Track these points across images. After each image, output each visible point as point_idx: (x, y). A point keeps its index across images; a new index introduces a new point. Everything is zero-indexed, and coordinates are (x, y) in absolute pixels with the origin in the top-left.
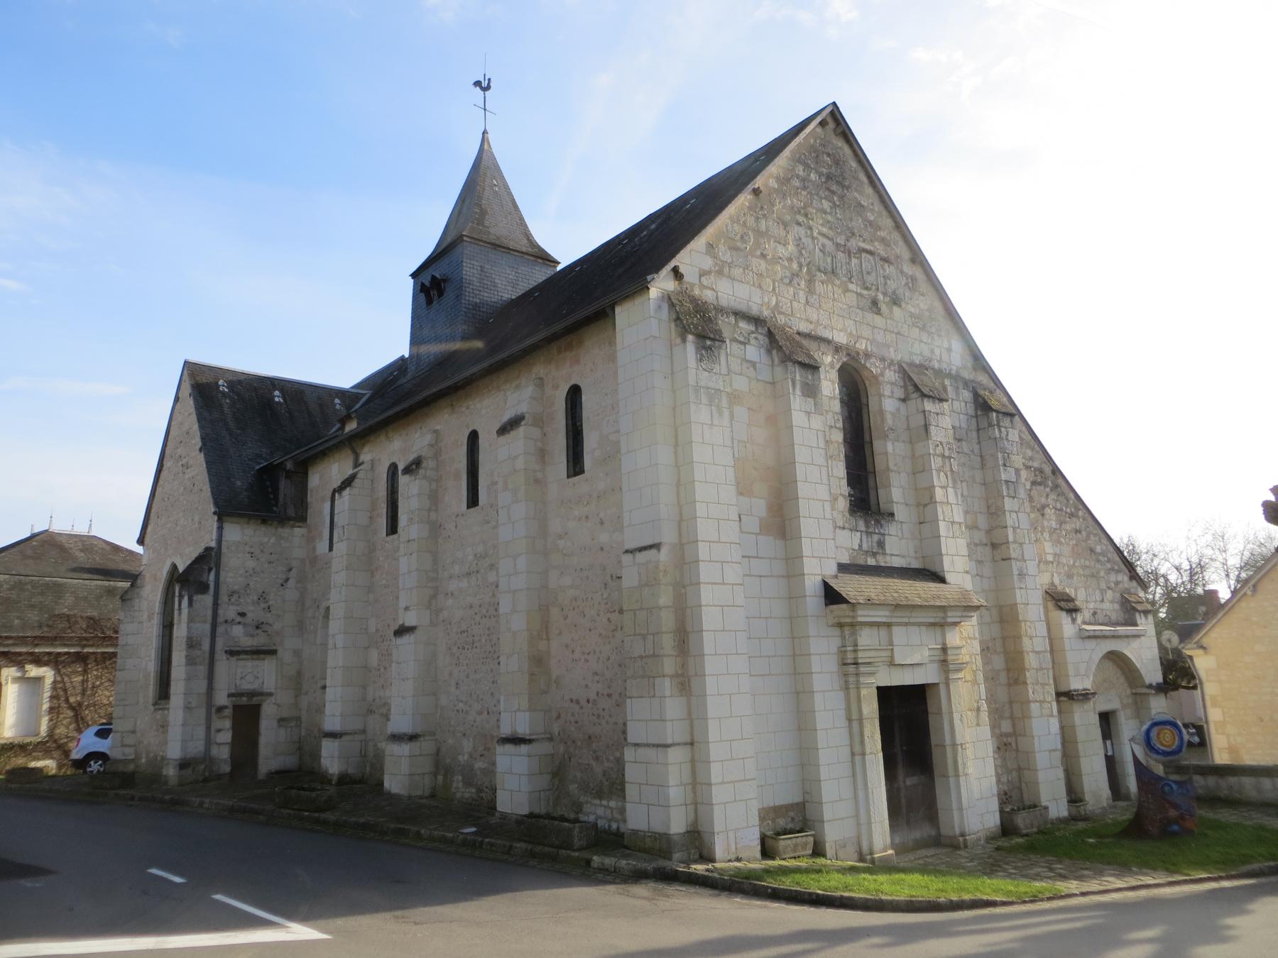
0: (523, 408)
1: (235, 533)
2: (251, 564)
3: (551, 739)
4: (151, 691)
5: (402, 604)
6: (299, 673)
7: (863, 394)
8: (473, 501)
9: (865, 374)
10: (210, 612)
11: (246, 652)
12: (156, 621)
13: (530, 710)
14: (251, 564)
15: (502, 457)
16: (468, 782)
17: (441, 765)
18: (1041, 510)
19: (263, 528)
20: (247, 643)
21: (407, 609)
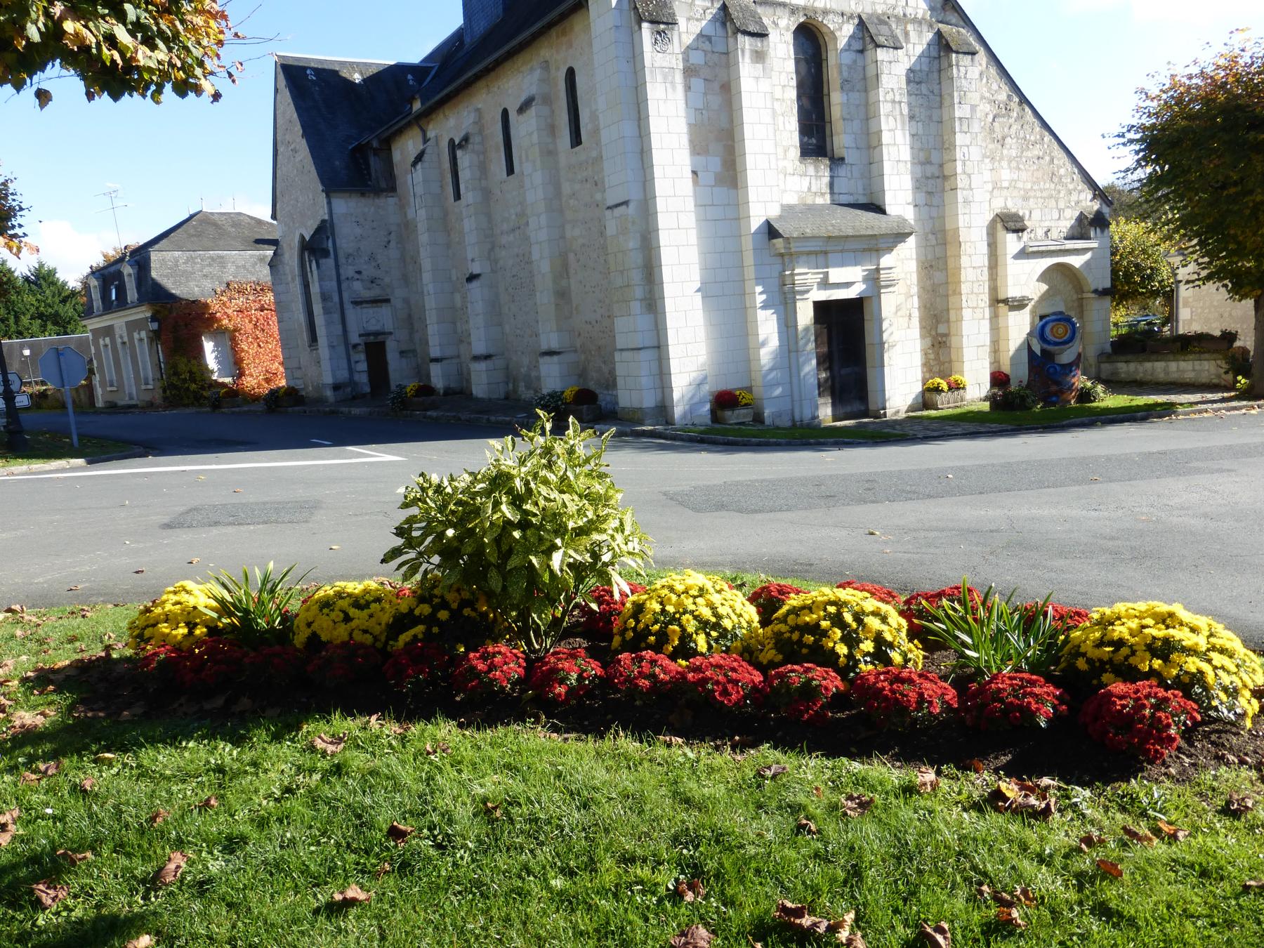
0: (533, 90)
1: (344, 206)
2: (358, 231)
3: (576, 351)
4: (305, 336)
5: (470, 257)
6: (410, 316)
7: (823, 49)
8: (510, 170)
9: (824, 30)
10: (334, 272)
11: (367, 302)
12: (298, 281)
14: (358, 231)
15: (526, 129)
16: (528, 388)
17: (510, 376)
18: (1002, 142)
19: (363, 200)
20: (367, 294)
21: (473, 260)
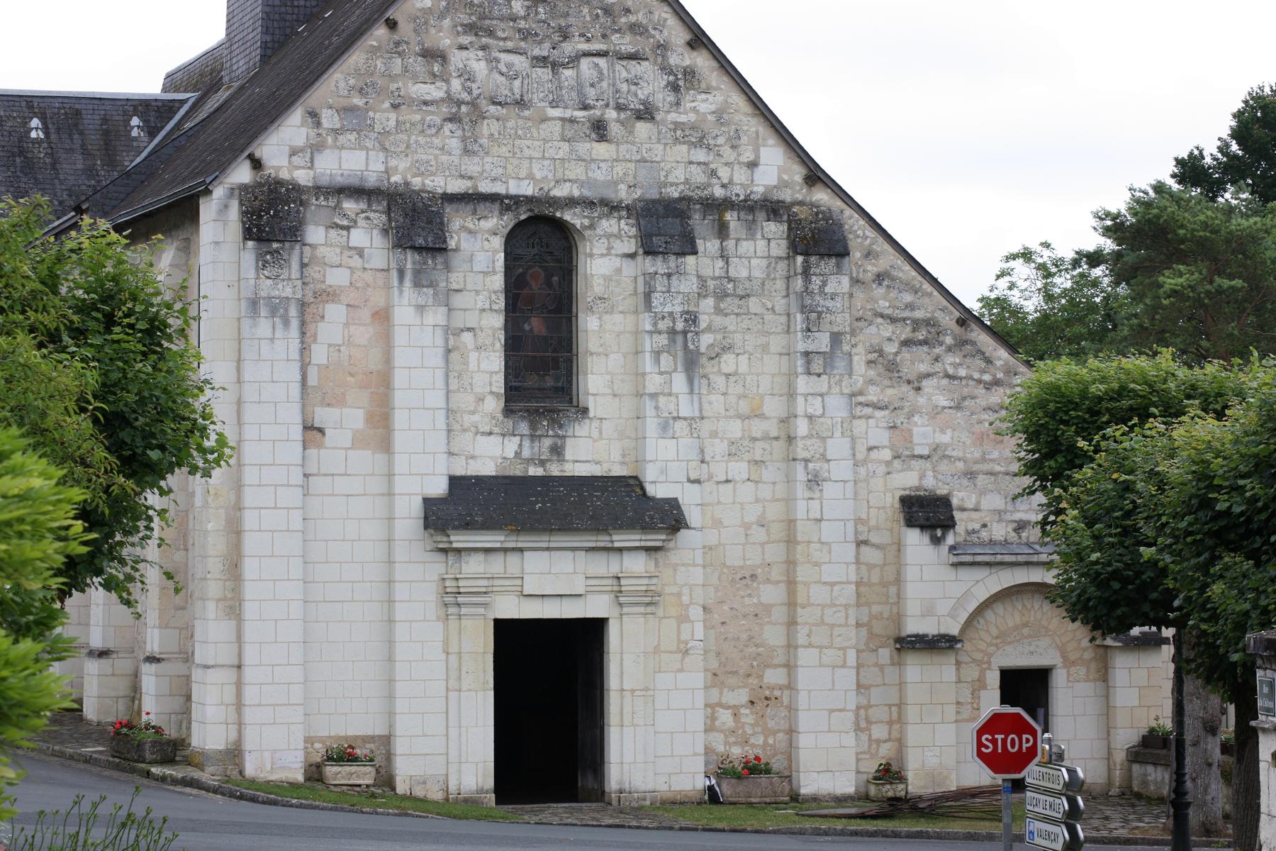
13: (160, 627)
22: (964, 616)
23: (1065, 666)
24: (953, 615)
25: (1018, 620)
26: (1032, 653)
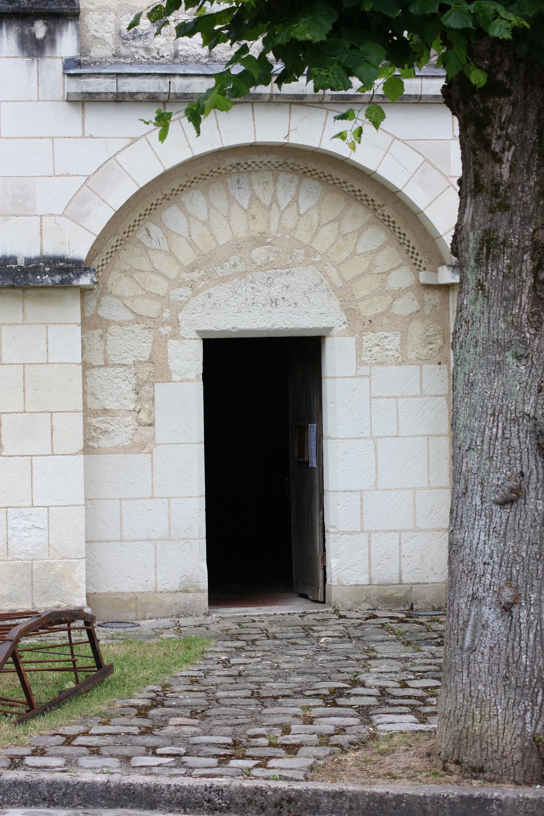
22: (100, 218)
23: (351, 331)
24: (73, 212)
25: (240, 227)
26: (274, 302)
